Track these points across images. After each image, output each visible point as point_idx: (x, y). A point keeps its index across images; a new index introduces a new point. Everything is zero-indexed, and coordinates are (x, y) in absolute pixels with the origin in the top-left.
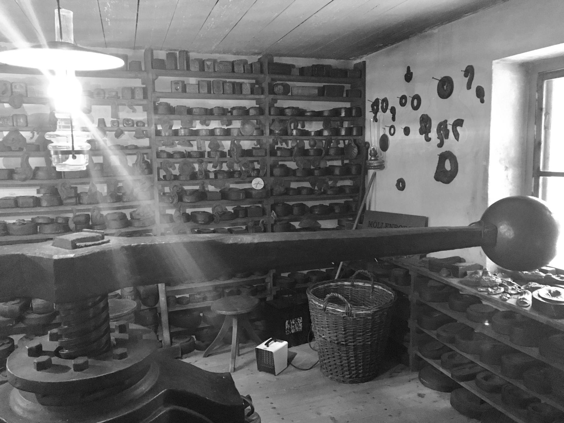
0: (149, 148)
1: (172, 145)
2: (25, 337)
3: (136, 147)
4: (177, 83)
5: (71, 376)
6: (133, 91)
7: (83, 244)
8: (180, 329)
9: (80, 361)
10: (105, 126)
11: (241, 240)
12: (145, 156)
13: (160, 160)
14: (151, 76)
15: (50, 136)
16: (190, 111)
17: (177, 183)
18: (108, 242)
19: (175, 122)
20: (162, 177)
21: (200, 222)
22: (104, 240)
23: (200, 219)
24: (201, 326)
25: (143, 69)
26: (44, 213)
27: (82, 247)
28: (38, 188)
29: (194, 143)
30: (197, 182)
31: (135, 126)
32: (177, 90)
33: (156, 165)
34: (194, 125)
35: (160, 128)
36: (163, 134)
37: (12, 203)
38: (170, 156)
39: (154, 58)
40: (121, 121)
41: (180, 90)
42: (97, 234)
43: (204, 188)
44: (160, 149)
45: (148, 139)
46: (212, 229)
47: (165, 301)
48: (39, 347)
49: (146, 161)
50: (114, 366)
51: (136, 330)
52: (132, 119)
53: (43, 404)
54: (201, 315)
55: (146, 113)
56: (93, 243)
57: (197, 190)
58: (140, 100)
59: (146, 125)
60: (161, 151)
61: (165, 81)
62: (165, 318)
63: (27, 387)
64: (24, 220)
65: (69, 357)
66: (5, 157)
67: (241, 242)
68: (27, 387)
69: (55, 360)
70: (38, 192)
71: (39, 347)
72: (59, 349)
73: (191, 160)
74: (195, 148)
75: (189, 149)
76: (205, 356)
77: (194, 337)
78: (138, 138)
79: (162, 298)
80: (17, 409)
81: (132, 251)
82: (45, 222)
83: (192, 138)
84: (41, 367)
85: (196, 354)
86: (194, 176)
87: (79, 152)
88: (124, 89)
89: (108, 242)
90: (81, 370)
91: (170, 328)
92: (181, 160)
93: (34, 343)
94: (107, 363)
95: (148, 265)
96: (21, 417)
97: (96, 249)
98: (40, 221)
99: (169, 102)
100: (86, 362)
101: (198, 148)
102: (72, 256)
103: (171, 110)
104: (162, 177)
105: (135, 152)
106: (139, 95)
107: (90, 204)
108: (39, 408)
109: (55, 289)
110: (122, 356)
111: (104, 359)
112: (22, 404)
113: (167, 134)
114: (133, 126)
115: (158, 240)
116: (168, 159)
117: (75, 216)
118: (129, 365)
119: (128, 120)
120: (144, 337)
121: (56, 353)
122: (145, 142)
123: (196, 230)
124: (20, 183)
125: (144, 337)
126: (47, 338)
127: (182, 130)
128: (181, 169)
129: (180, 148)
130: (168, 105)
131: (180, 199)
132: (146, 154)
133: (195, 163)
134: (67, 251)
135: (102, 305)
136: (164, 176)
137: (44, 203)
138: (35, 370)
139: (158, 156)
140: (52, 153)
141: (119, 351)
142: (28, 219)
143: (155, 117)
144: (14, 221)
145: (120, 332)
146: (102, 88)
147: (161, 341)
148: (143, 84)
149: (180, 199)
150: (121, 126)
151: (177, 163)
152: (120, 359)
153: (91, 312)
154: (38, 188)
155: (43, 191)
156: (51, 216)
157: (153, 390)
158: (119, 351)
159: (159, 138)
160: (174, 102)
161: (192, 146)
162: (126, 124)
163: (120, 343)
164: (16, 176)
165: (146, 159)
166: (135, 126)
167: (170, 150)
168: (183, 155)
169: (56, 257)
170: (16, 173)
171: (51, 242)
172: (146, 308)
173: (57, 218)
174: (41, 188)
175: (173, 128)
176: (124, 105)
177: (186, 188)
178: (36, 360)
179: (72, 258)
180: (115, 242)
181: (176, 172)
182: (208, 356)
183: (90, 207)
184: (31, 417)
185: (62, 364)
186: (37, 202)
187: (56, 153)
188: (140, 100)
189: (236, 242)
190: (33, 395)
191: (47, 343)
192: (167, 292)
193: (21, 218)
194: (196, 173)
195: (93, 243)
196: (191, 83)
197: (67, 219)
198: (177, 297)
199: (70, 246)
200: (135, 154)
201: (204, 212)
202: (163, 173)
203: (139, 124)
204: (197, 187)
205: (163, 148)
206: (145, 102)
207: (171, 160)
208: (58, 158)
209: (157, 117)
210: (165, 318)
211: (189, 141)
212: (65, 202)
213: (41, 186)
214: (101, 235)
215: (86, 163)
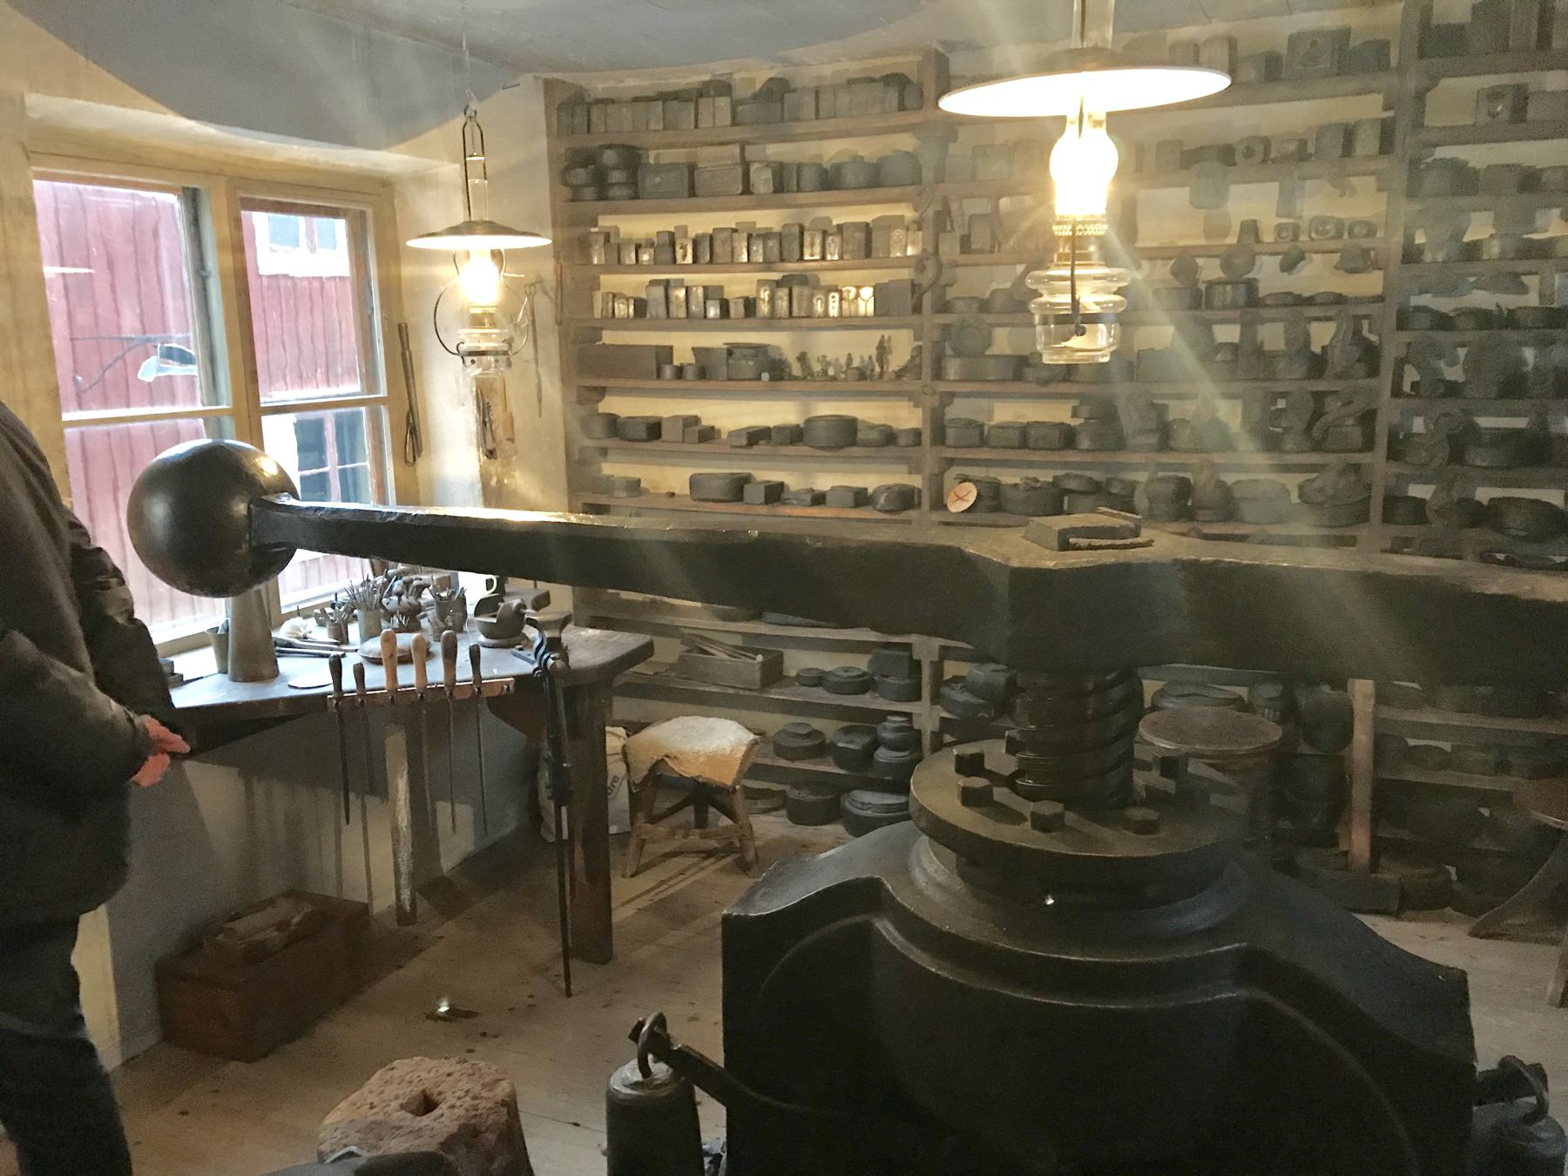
0: (1380, 299)
1: (1452, 289)
2: (266, 493)
3: (1339, 300)
4: (1495, 95)
5: (1008, 834)
6: (1348, 134)
7: (1083, 542)
8: (1404, 835)
9: (1049, 808)
10: (1258, 241)
11: (1532, 590)
12: (1365, 323)
13: (1406, 336)
14: (1412, 83)
15: (1039, 280)
16: (1529, 181)
17: (1451, 406)
18: (1149, 544)
19: (1475, 216)
20: (1407, 388)
21: (1513, 532)
22: (1139, 540)
23: (1516, 522)
24: (1477, 844)
25: (1394, 62)
26: (1081, 464)
27: (1079, 548)
28: (1076, 403)
29: (1532, 281)
30: (1516, 405)
31: (1346, 236)
32: (1494, 115)
33: (1391, 353)
34: (1539, 223)
35: (1420, 239)
36: (1428, 257)
37: (1014, 436)
38: (1443, 322)
39: (1435, 22)
40: (1304, 225)
41: (1505, 115)
42: (1125, 523)
43: (1544, 425)
44: (1416, 301)
45: (1381, 273)
46: (1559, 559)
47: (1370, 746)
48: (978, 759)
49: (1366, 340)
50: (1121, 845)
51: (1201, 778)
52: (1337, 215)
53: (962, 876)
54: (1485, 812)
55: (1384, 196)
56: (1109, 542)
57: (1521, 431)
58: (1369, 158)
59: (1380, 234)
60: (1417, 309)
61: (1458, 94)
62: (1361, 794)
63: (942, 833)
64: (1036, 480)
65: (1031, 795)
66: (1012, 325)
67: (1532, 597)
68: (942, 833)
69: (1001, 794)
70: (1075, 415)
71: (978, 759)
72: (1015, 775)
73: (1514, 336)
74: (1532, 300)
75: (1509, 301)
76: (1475, 934)
77: (1452, 870)
78: (1353, 271)
79: (1362, 737)
80: (917, 874)
81: (1203, 578)
82: (1082, 489)
83: (1523, 266)
84: (970, 798)
85: (1447, 921)
86: (1513, 387)
87: (1094, 319)
88: (1323, 130)
89: (1149, 544)
90: (1045, 830)
91: (1375, 823)
92: (1476, 336)
93: (970, 749)
94: (1107, 833)
95: (1241, 620)
96: (921, 893)
97: (1108, 557)
98: (1073, 485)
99: (1462, 157)
100: (1060, 816)
101: (1541, 296)
102: (1050, 564)
103: (1465, 181)
104: (1407, 388)
105: (1332, 311)
106: (1367, 143)
107: (1195, 451)
108: (958, 885)
109: (1008, 633)
110: (1146, 828)
111: (1104, 822)
112: (931, 870)
113: (1440, 257)
114: (1339, 236)
115: (1279, 558)
116: (1431, 333)
117: (1151, 481)
118: (1153, 852)
119: (1323, 221)
120: (1216, 800)
121: (1010, 782)
122: (1370, 283)
123: (1501, 557)
124: (1036, 388)
125: (1216, 800)
126: (1000, 747)
127: (1495, 243)
128: (1473, 366)
129: (1482, 299)
130: (1458, 167)
131: (1457, 455)
132: (1366, 317)
133: (1526, 344)
134: (1047, 552)
135: (1117, 693)
136: (1414, 385)
137: (1085, 443)
138: (959, 803)
139: (1403, 321)
140: (1037, 319)
141: (1138, 814)
142: (1046, 476)
143: (1409, 208)
144: (1017, 480)
145: (1163, 774)
146: (1264, 133)
147: (1346, 853)
148: (1387, 108)
149: (1457, 455)
150: (1303, 238)
151: (1463, 345)
152: (1138, 831)
153: (1092, 704)
154: (1076, 403)
155: (1085, 411)
156: (1097, 476)
157: (1211, 934)
158: (1138, 814)
159: (1415, 270)
160: (1478, 156)
161: (1524, 290)
162: (1317, 232)
163: (1155, 798)
164: (1030, 373)
165: (1365, 333)
166: (1346, 236)
167: (1445, 305)
168: (1485, 319)
169: (1015, 563)
170: (1029, 366)
171: (1022, 531)
172: (1312, 751)
173: (1109, 481)
174: (1082, 403)
175: (1466, 239)
176: (1319, 177)
177: (1485, 422)
178: (963, 781)
179: (1050, 570)
180: (1165, 544)
181: (1455, 374)
182: (1488, 936)
183: (1193, 459)
184: (938, 897)
185: (1015, 806)
186: (1068, 438)
187: (1045, 321)
188: (1369, 158)
189: (1511, 591)
190: (951, 856)
191: (998, 757)
192: (1377, 722)
193: (1031, 473)
194: (1524, 377)
195: (1109, 542)
196: (1549, 89)
197: (1132, 485)
198: (1412, 742)
199: (1055, 544)
200: (1329, 319)
201: (1537, 502)
202: (1411, 375)
203: (1356, 230)
204: (1521, 423)
205: (1426, 300)
206: (1383, 164)
207: (1441, 336)
208: (1048, 333)
209: (1415, 206)
210: (1361, 794)
211: (1517, 275)
212: (1132, 442)
213: (1082, 398)
214: (1132, 525)
215: (1110, 345)
